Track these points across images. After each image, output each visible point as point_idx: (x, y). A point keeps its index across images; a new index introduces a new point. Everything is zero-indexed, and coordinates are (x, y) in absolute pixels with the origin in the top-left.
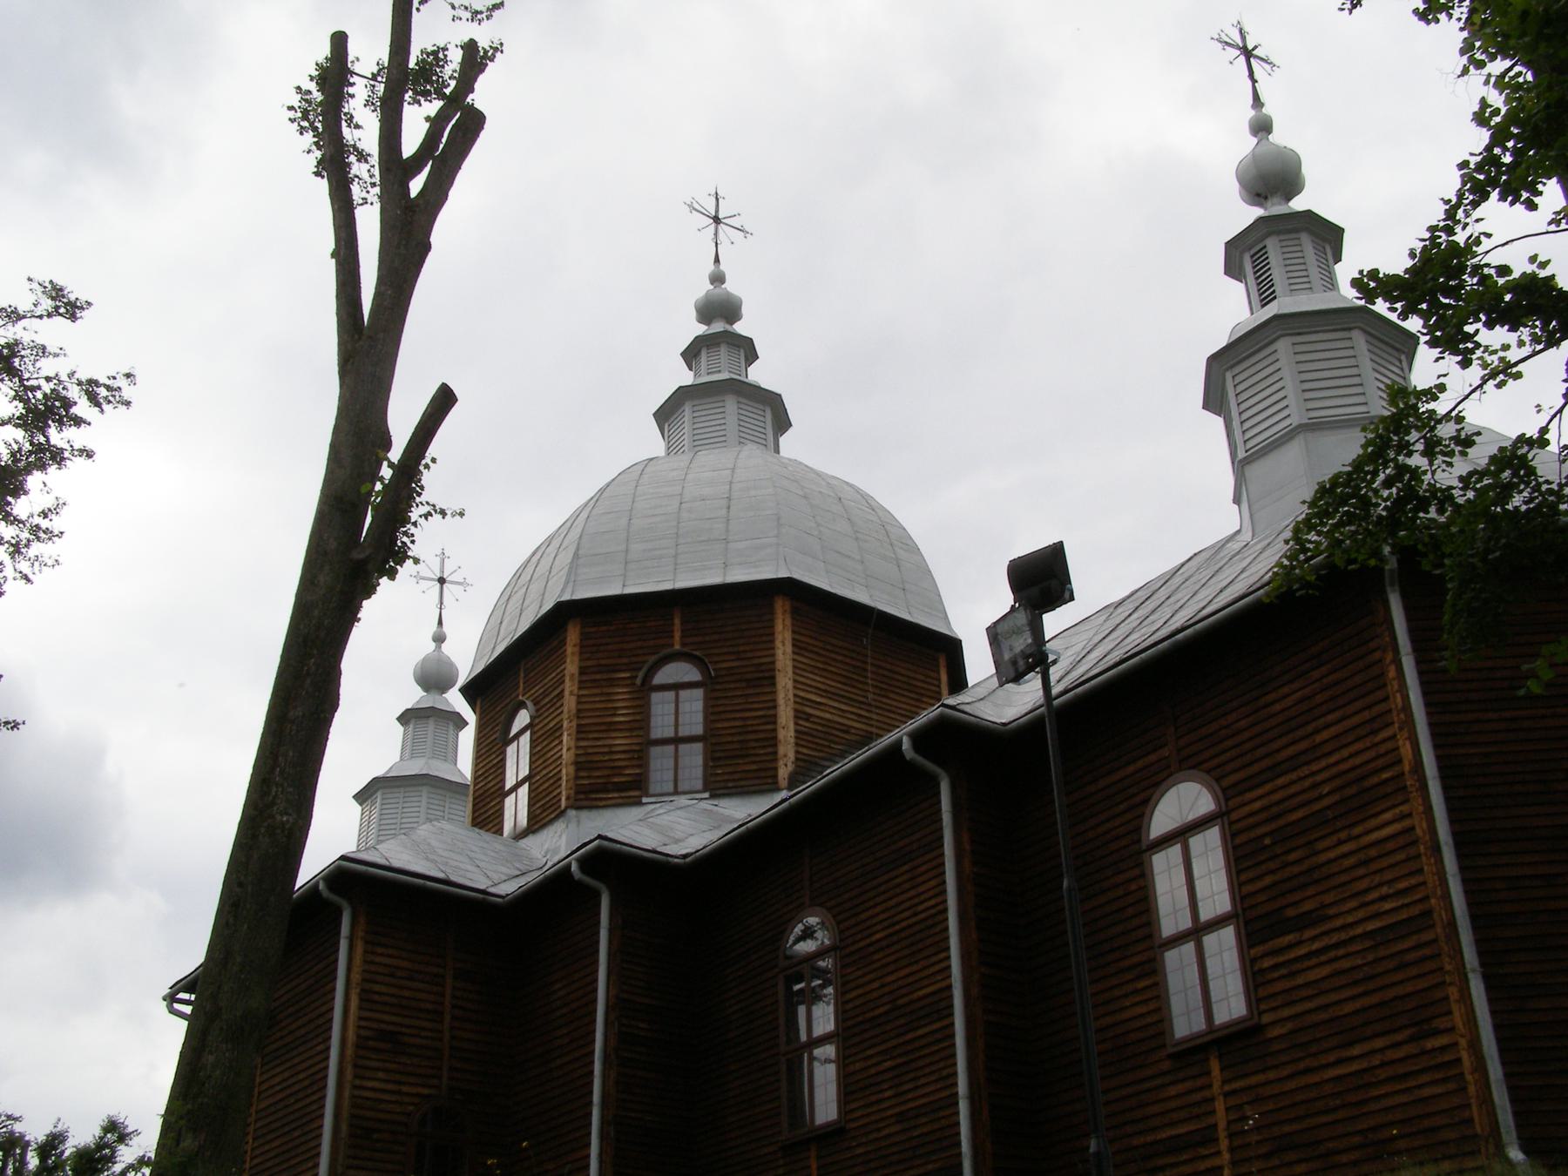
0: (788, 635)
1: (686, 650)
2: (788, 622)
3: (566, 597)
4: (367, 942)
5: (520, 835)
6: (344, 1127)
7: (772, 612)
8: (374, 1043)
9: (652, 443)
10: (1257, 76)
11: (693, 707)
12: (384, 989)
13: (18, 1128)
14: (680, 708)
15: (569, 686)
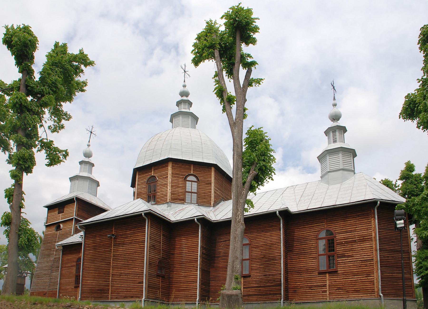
1: (194, 174)
8: (152, 247)
11: (195, 185)
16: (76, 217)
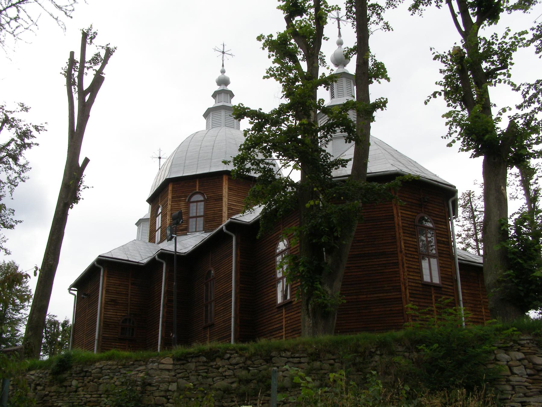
0: (227, 186)
2: (227, 182)
3: (168, 177)
4: (107, 277)
5: (159, 243)
6: (102, 324)
7: (222, 180)
8: (110, 303)
9: (201, 124)
10: (341, 27)
12: (112, 289)
13: (56, 319)
14: (197, 208)
15: (169, 202)
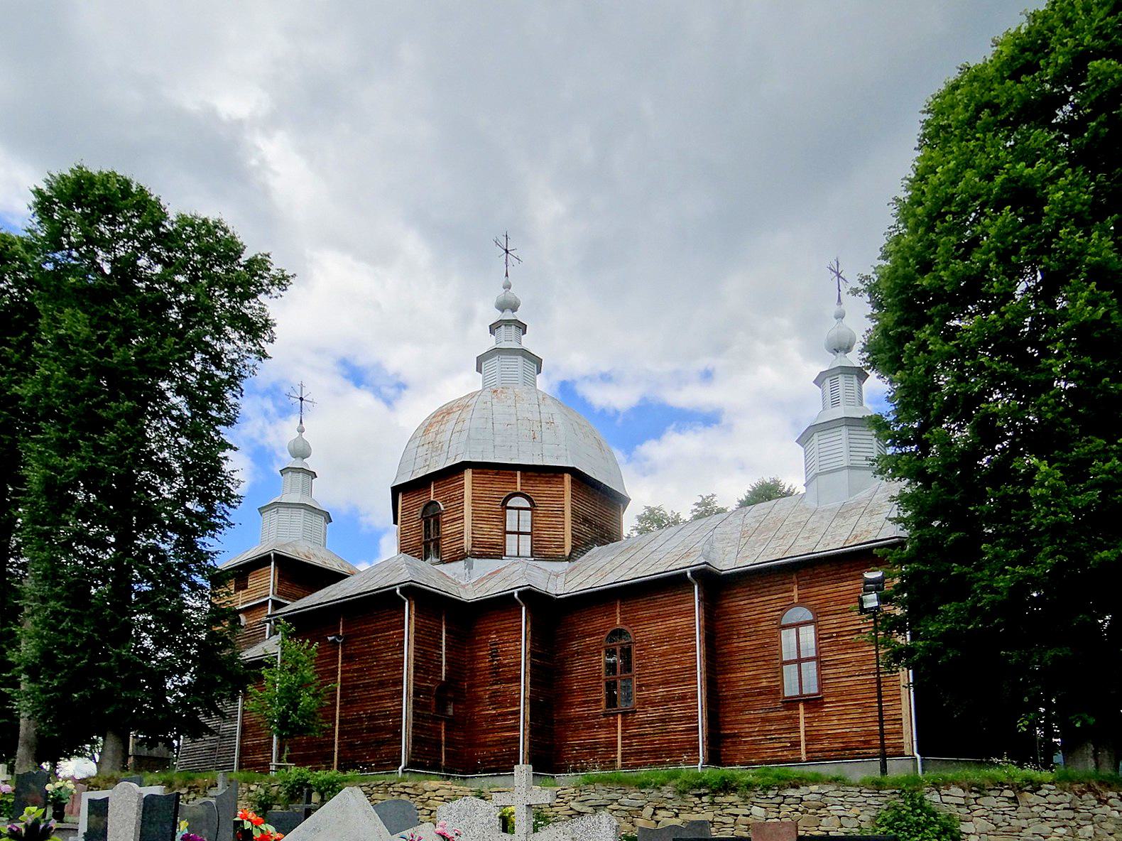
1: (523, 492)
16: (275, 598)
